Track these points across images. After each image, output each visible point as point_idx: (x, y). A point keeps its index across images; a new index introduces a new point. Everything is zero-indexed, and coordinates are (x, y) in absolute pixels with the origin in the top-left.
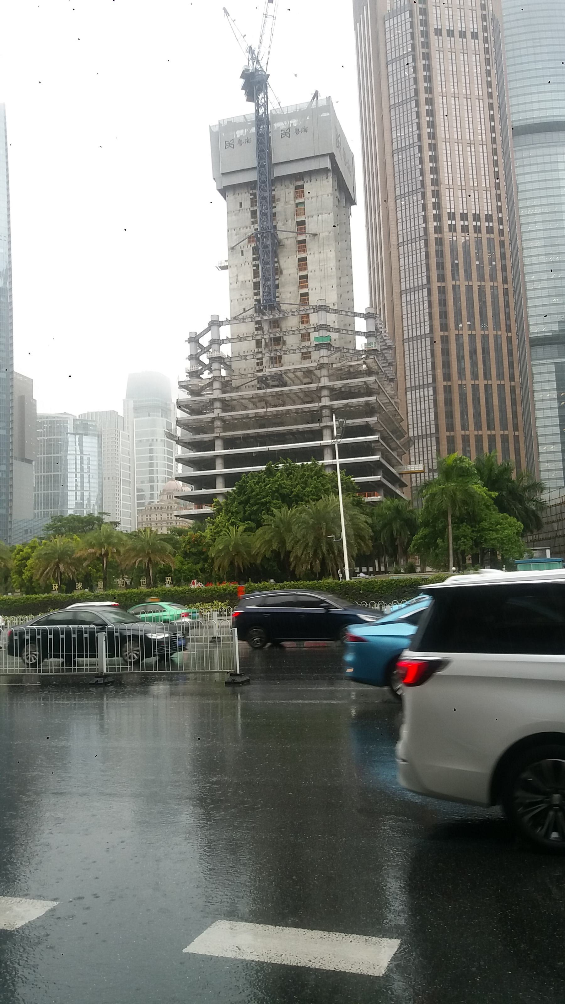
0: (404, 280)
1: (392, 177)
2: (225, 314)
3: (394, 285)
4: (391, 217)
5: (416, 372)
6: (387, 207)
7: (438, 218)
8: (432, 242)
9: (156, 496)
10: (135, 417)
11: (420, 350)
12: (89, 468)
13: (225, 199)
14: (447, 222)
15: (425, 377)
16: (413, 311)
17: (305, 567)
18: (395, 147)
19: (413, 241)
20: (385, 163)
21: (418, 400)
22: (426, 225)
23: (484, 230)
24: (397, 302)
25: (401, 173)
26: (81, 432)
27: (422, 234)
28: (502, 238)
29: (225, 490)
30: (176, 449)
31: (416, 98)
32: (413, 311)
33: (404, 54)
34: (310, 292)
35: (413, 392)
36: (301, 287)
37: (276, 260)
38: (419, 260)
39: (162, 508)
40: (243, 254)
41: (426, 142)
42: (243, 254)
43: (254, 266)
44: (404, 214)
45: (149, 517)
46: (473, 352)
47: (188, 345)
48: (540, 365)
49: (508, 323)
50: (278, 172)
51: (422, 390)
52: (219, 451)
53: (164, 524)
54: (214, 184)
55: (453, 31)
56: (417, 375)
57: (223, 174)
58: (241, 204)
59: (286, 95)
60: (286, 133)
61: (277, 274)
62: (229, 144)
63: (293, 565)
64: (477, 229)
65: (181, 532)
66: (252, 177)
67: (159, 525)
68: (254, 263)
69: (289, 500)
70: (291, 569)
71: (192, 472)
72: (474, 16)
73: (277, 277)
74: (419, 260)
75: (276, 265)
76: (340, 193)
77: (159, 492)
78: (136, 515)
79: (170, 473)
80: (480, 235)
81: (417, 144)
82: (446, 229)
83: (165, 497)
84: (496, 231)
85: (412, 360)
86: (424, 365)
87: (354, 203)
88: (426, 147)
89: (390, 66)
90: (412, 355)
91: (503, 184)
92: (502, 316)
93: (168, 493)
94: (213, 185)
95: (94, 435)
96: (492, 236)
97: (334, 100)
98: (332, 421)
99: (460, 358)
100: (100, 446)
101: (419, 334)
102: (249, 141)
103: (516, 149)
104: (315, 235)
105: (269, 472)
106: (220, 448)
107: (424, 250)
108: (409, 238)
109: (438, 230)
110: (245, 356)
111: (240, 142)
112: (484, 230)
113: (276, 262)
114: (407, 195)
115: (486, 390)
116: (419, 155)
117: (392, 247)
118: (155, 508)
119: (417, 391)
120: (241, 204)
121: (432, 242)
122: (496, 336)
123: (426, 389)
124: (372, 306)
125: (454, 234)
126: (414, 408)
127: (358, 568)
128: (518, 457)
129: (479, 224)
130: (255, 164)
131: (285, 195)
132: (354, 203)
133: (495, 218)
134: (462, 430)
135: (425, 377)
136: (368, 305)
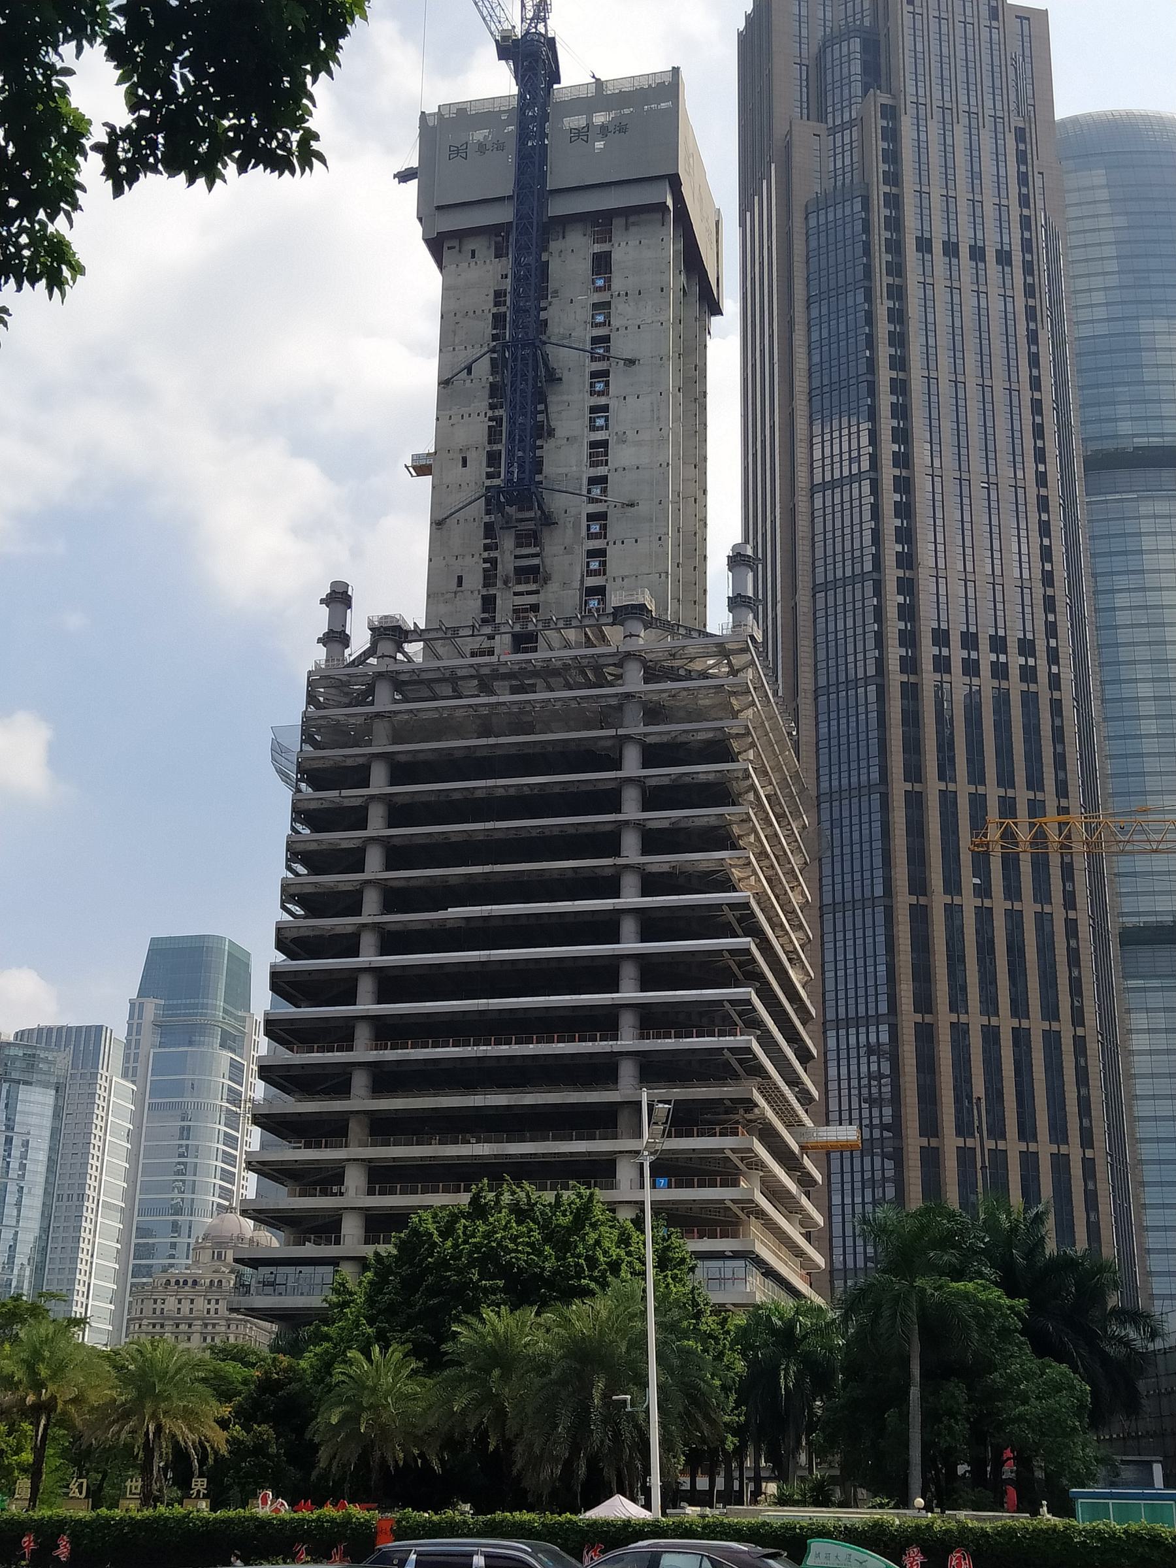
0: (822, 613)
1: (808, 542)
2: (415, 614)
3: (799, 548)
4: (796, 251)
5: (851, 985)
6: (795, 608)
7: (909, 639)
8: (895, 692)
9: (181, 1250)
10: (153, 1046)
11: (847, 531)
12: (23, 1167)
13: (441, 266)
14: (928, 650)
15: (871, 999)
16: (846, 841)
17: (550, 1472)
18: (820, 579)
19: (852, 685)
20: (793, 510)
21: (853, 1053)
22: (878, 550)
23: (1014, 672)
24: (802, 506)
25: (830, 560)
26: (15, 1075)
27: (871, 671)
28: (1056, 695)
29: (373, 1056)
30: (249, 1133)
31: (872, 475)
32: (846, 841)
33: (835, 126)
34: (613, 404)
35: (842, 1032)
36: (593, 464)
37: (541, 407)
38: (862, 728)
39: (195, 1283)
40: (465, 464)
41: (888, 473)
42: (465, 464)
43: (491, 419)
44: (834, 756)
45: (159, 1306)
46: (986, 948)
47: (325, 610)
48: (1144, 989)
49: (1073, 943)
50: (559, 207)
51: (862, 1030)
52: (369, 957)
53: (197, 1326)
54: (418, 229)
55: (975, 635)
56: (851, 993)
57: (439, 208)
58: (460, 579)
59: (588, 59)
60: (582, 135)
61: (540, 437)
62: (459, 152)
63: (519, 1465)
64: (1000, 671)
65: (239, 1355)
66: (504, 215)
67: (183, 1327)
68: (485, 555)
69: (525, 1290)
70: (515, 1472)
71: (285, 1199)
72: (1027, 601)
73: (539, 443)
74: (862, 728)
75: (540, 417)
76: (688, 278)
77: (192, 1241)
78: (128, 1299)
79: (226, 1193)
80: (1004, 684)
81: (867, 475)
82: (927, 665)
83: (206, 1256)
84: (1043, 677)
85: (841, 987)
86: (870, 969)
87: (716, 310)
88: (887, 483)
89: (818, 498)
90: (840, 944)
91: (1061, 574)
92: (1072, 1107)
93: (217, 1243)
94: (416, 230)
95: (46, 1085)
96: (1033, 687)
97: (684, 74)
98: (642, 1187)
99: (956, 959)
100: (57, 1114)
101: (848, 573)
102: (500, 147)
103: (1132, 983)
104: (631, 362)
105: (478, 1210)
106: (372, 950)
107: (875, 707)
108: (842, 678)
109: (910, 665)
110: (455, 630)
111: (482, 148)
112: (1014, 672)
113: (541, 412)
114: (840, 583)
115: (1016, 1042)
116: (866, 306)
117: (801, 694)
118: (177, 1283)
119: (852, 1031)
120: (460, 579)
121: (895, 692)
122: (1040, 917)
123: (872, 1029)
124: (746, 541)
125: (946, 677)
126: (844, 1070)
127: (688, 1480)
128: (1083, 1091)
129: (1002, 658)
130: (507, 189)
131: (570, 259)
132: (716, 310)
133: (1041, 646)
134: (951, 1011)
135: (871, 999)
136: (739, 539)
